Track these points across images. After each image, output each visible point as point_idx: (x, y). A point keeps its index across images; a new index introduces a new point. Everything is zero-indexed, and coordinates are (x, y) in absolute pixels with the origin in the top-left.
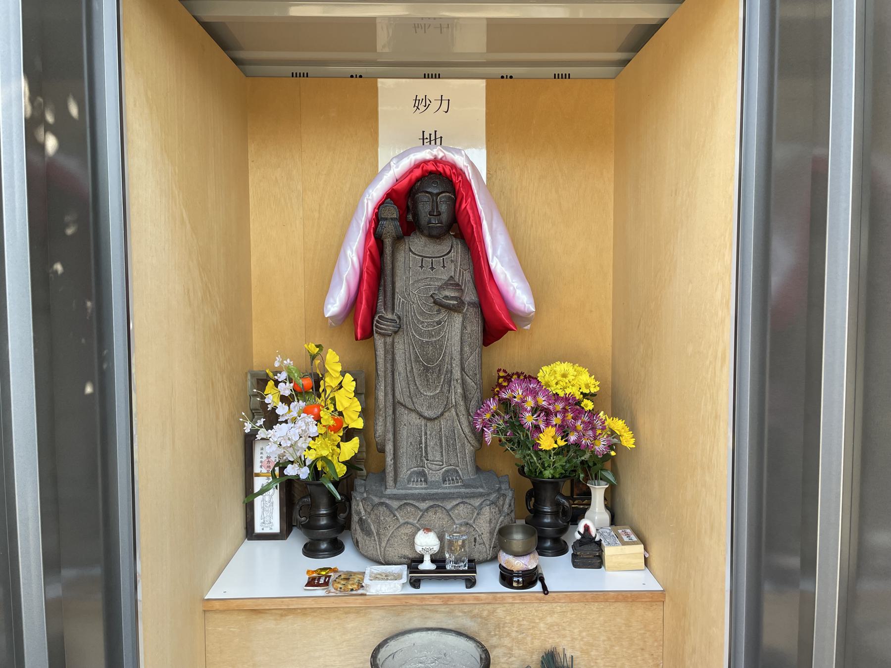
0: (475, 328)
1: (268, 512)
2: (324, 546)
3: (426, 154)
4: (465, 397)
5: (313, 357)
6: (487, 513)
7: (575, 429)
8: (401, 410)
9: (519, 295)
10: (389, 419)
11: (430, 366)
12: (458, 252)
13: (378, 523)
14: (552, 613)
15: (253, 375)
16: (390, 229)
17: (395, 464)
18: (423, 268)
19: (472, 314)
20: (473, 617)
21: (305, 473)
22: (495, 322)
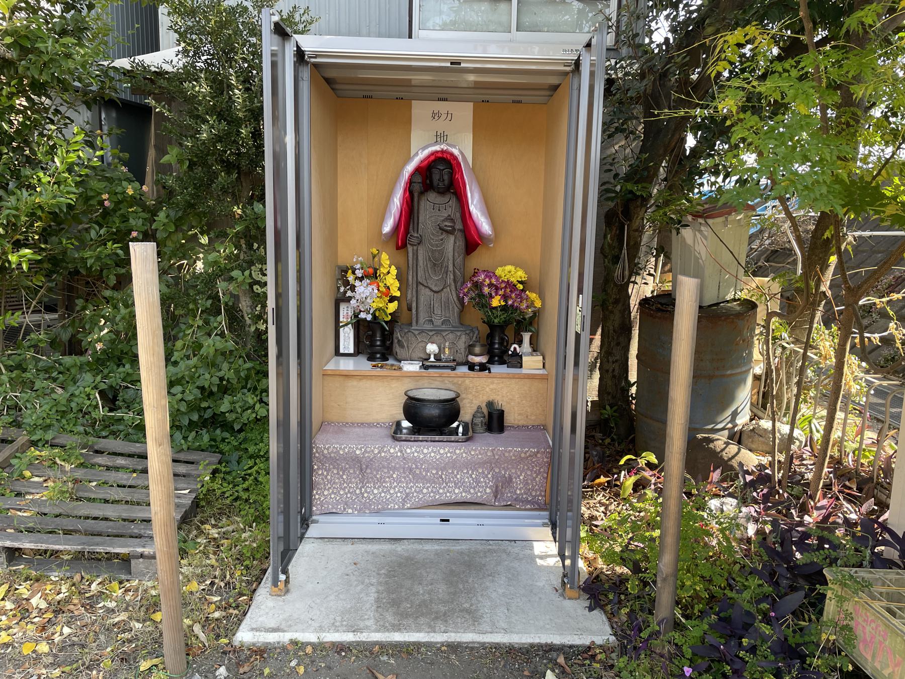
0: (461, 243)
1: (347, 341)
2: (378, 356)
3: (437, 148)
4: (455, 281)
5: (374, 257)
6: (463, 338)
7: (511, 298)
8: (420, 287)
9: (485, 227)
10: (414, 290)
11: (437, 263)
12: (453, 202)
13: (408, 341)
14: (492, 383)
15: (339, 267)
16: (417, 188)
17: (417, 314)
18: (434, 211)
19: (459, 235)
20: (454, 384)
21: (369, 317)
22: (472, 241)
